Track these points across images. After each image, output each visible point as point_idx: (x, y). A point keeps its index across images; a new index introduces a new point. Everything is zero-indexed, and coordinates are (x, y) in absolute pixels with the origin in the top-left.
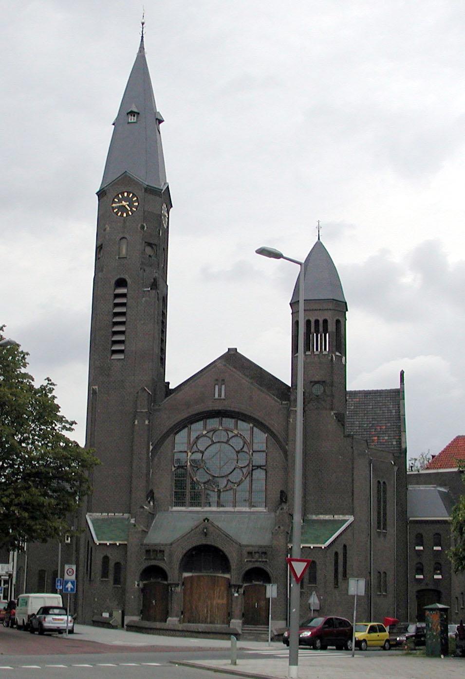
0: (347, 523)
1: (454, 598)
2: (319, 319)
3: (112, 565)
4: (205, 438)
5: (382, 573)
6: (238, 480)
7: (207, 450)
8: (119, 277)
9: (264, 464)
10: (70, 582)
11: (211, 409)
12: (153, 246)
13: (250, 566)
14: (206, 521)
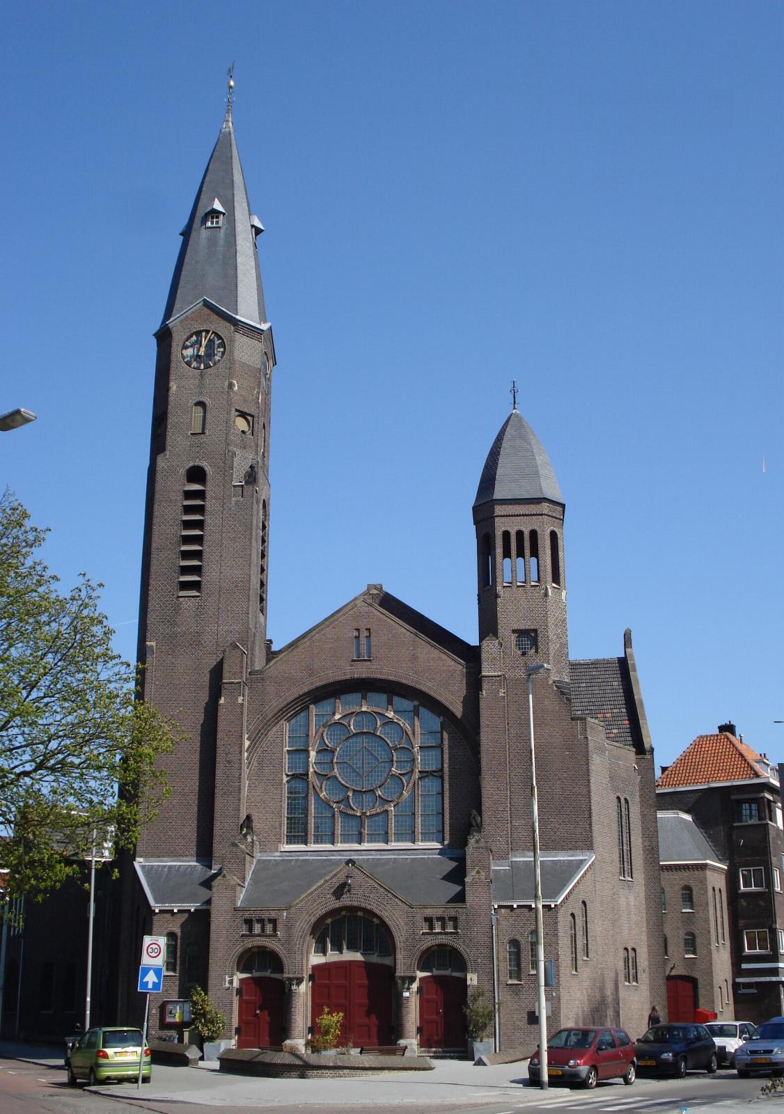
2: (523, 529)
5: (630, 950)
8: (191, 464)
10: (152, 972)
11: (348, 677)
13: (430, 942)
14: (350, 865)
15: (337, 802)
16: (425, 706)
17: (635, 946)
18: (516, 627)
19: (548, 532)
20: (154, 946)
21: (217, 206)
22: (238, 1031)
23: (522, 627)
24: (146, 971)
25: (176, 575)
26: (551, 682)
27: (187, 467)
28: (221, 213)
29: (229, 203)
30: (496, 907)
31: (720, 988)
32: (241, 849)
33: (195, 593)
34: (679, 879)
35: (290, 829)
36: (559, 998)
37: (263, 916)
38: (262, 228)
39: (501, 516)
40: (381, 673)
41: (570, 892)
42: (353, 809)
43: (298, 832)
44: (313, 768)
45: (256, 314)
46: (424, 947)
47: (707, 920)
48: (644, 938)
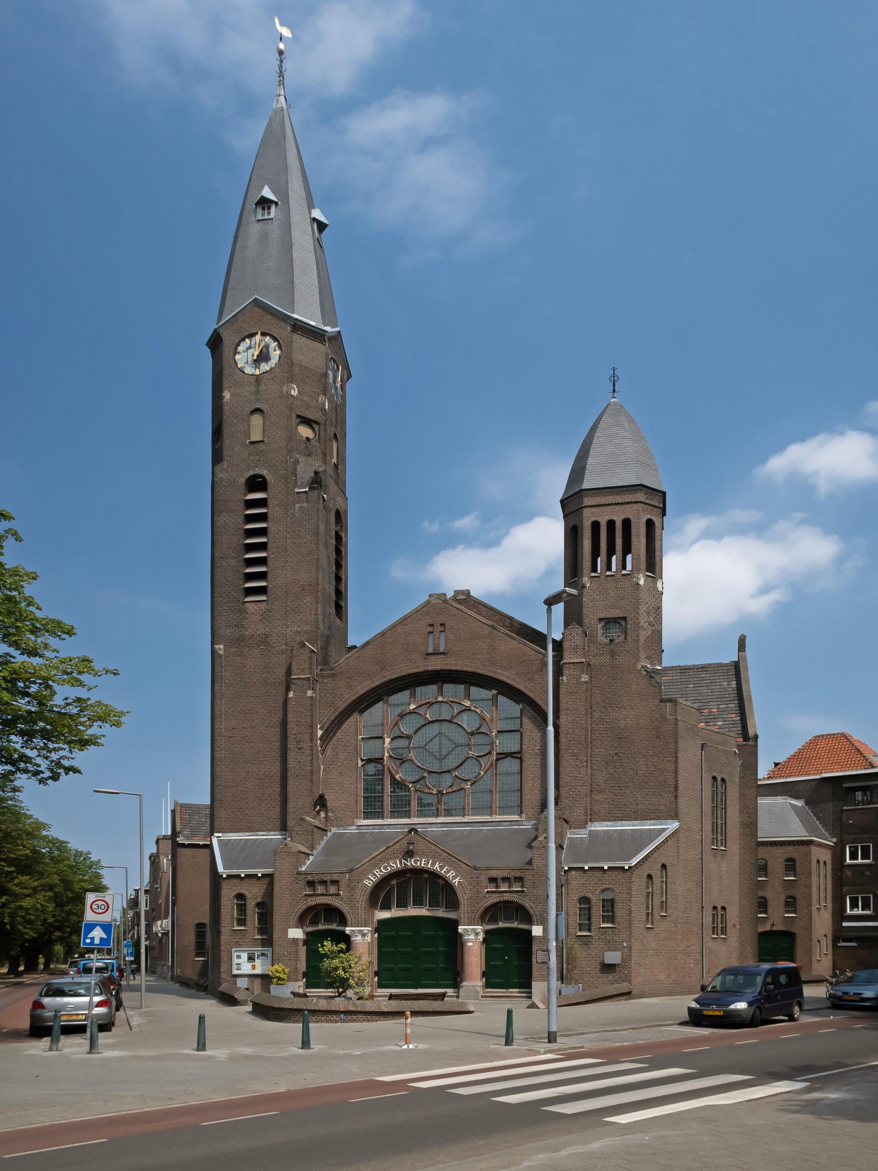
0: (664, 834)
1: (815, 941)
2: (615, 518)
3: (251, 904)
4: (415, 715)
6: (472, 777)
7: (420, 733)
9: (517, 749)
11: (421, 670)
12: (315, 426)
13: (494, 899)
15: (413, 783)
16: (504, 695)
17: (725, 905)
18: (603, 616)
19: (644, 520)
20: (100, 903)
21: (267, 193)
22: (305, 975)
23: (609, 615)
24: (91, 927)
25: (241, 582)
26: (639, 667)
27: (247, 477)
28: (272, 202)
29: (282, 190)
30: (566, 868)
31: (819, 941)
32: (309, 824)
33: (264, 598)
34: (781, 854)
35: (366, 806)
36: (630, 948)
37: (325, 879)
38: (326, 222)
39: (591, 506)
40: (456, 665)
41: (648, 856)
42: (429, 788)
43: (373, 809)
44: (388, 752)
45: (319, 314)
46: (488, 904)
47: (809, 887)
48: (736, 898)
